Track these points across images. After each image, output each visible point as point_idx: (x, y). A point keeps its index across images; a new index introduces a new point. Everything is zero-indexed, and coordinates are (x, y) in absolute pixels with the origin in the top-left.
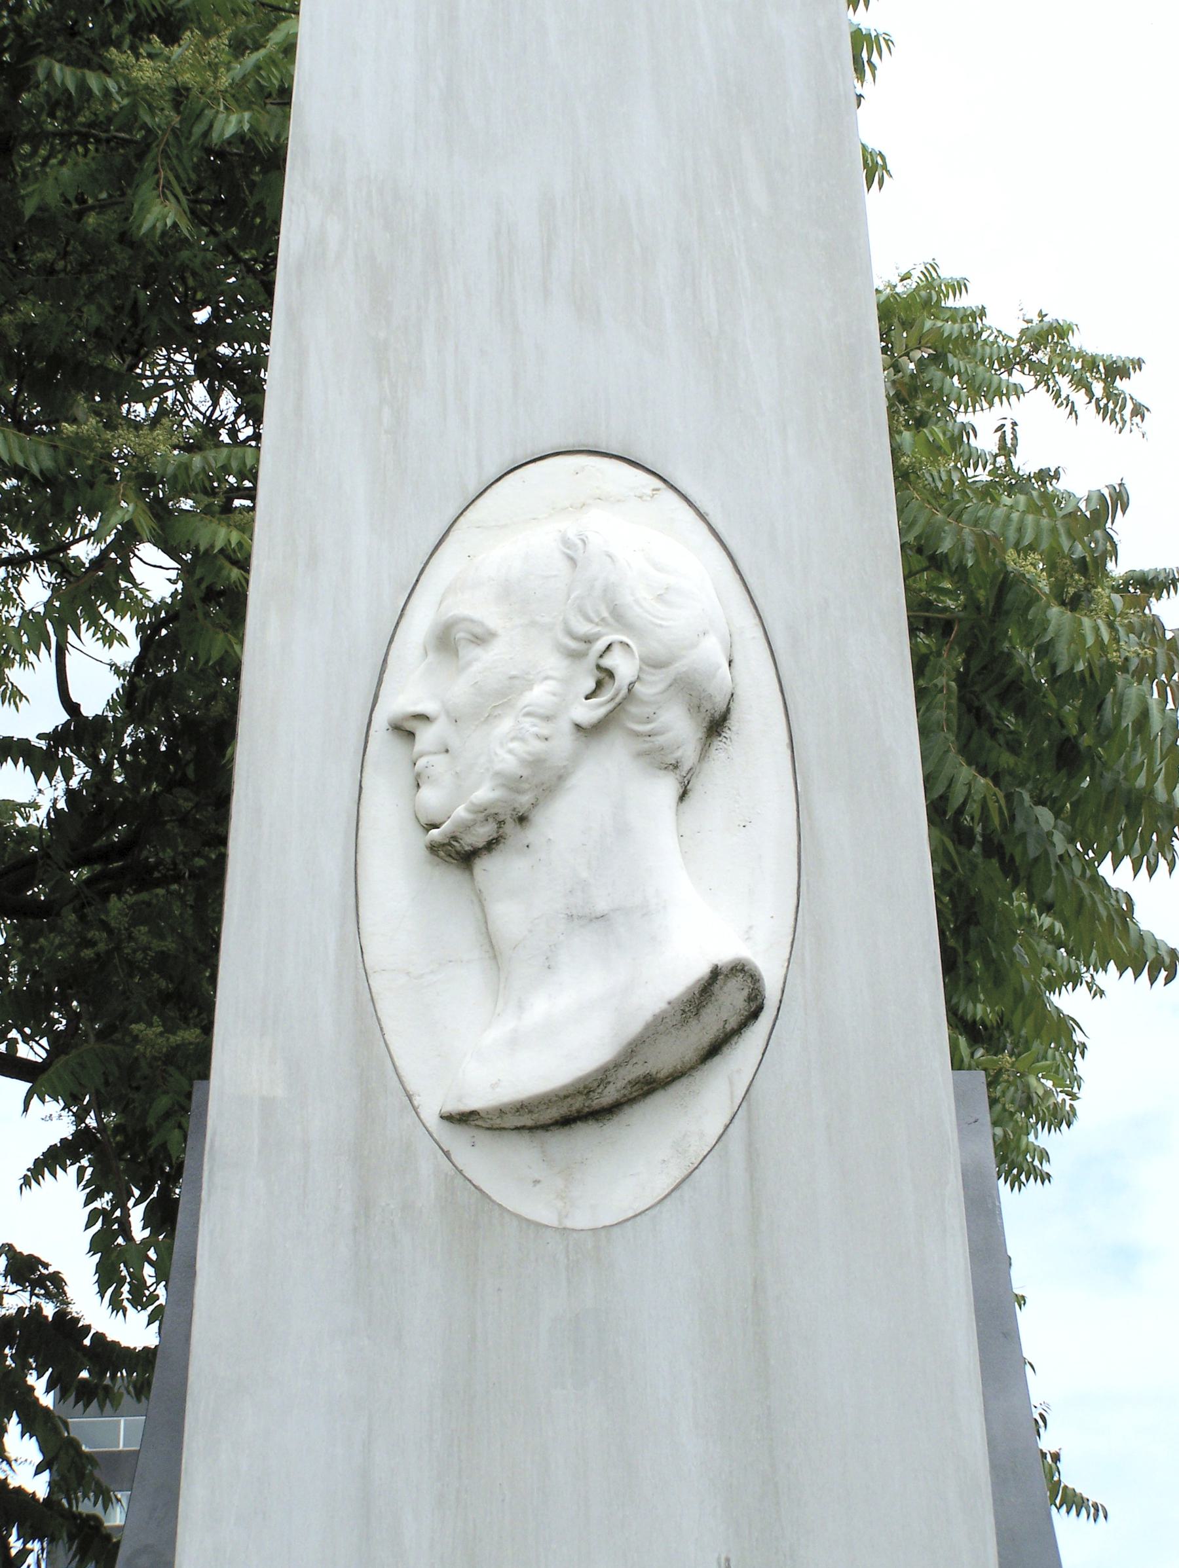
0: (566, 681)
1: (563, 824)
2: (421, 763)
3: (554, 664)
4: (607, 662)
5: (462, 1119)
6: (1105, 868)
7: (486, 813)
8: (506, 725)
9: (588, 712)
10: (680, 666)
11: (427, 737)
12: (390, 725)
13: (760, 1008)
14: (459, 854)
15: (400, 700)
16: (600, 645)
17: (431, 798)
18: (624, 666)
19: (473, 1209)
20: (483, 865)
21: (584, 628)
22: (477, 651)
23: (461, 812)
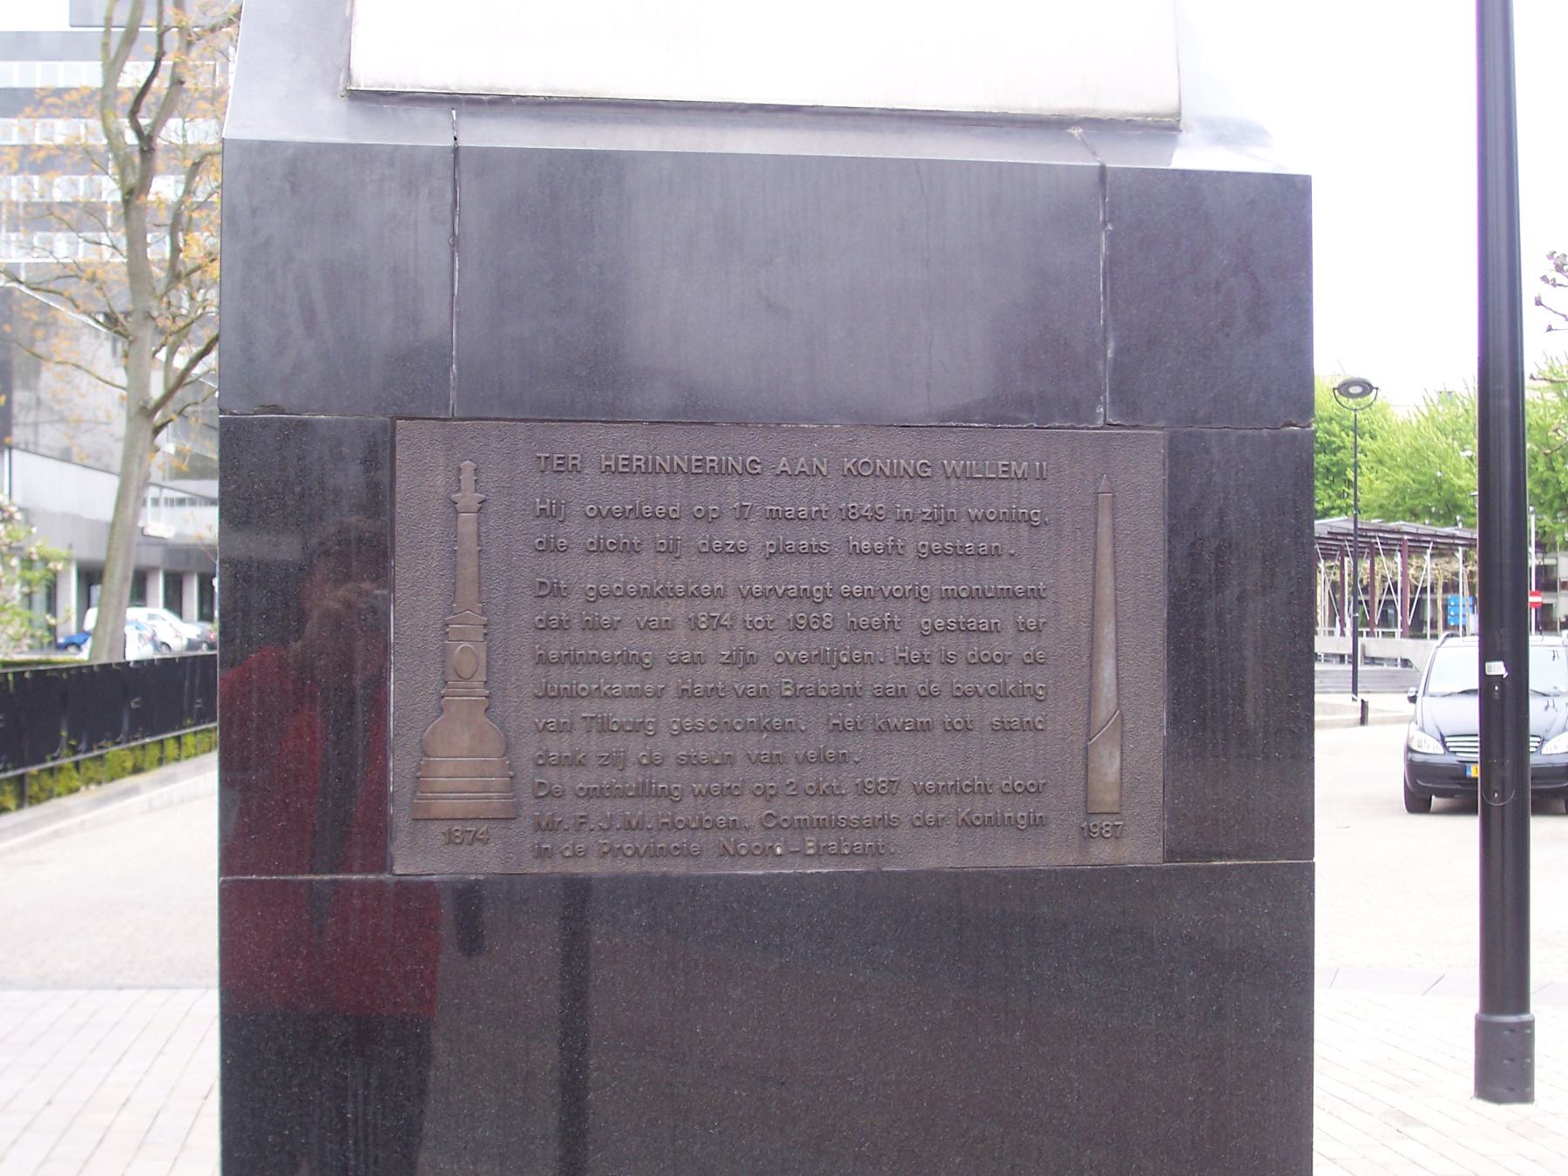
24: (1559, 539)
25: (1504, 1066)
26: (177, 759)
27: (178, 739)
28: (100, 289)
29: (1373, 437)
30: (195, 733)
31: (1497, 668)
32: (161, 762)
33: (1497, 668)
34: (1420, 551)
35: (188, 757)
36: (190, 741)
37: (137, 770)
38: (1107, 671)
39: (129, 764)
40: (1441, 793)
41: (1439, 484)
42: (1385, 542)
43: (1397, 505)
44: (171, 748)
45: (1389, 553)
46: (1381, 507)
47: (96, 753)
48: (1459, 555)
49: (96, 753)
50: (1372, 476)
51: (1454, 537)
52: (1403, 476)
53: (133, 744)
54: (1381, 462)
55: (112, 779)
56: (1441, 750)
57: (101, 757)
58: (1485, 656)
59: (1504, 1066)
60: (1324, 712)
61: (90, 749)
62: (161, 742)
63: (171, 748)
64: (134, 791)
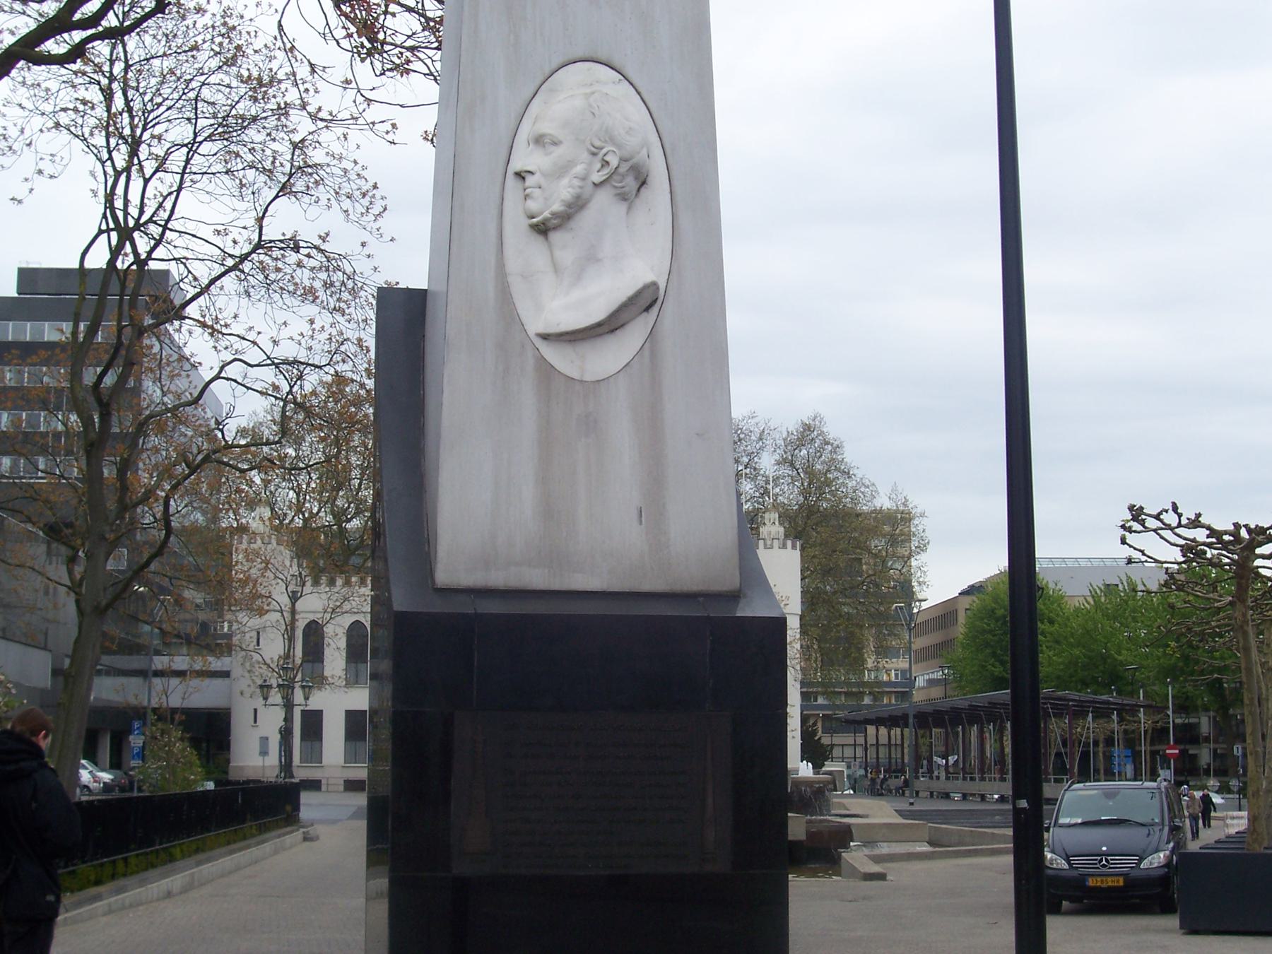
0: (590, 164)
1: (586, 219)
2: (528, 191)
3: (585, 156)
4: (607, 158)
5: (545, 337)
6: (111, 777)
7: (555, 215)
8: (565, 181)
9: (597, 177)
10: (635, 160)
11: (530, 180)
12: (807, 433)
13: (655, 301)
14: (542, 229)
15: (517, 164)
16: (604, 151)
17: (533, 205)
18: (614, 161)
19: (546, 371)
20: (555, 236)
21: (598, 143)
22: (553, 148)
23: (546, 214)
24: (1199, 702)
25: (256, 710)
26: (125, 875)
27: (125, 859)
28: (51, 509)
29: (1051, 622)
30: (137, 855)
31: (1023, 804)
32: (113, 877)
33: (1023, 804)
34: (1084, 715)
35: (132, 874)
36: (133, 861)
37: (98, 882)
38: (710, 801)
39: (92, 878)
40: (1071, 900)
41: (1104, 658)
42: (1054, 706)
43: (1071, 676)
44: (120, 866)
45: (1059, 715)
46: (1058, 677)
47: (71, 868)
48: (1115, 717)
49: (71, 868)
50: (1051, 653)
51: (1108, 703)
52: (1076, 652)
53: (95, 863)
54: (1057, 642)
55: (80, 889)
56: (1066, 866)
57: (74, 871)
58: (1017, 795)
59: (256, 710)
60: (1002, 839)
61: (66, 866)
62: (114, 862)
63: (120, 866)
64: (98, 898)
